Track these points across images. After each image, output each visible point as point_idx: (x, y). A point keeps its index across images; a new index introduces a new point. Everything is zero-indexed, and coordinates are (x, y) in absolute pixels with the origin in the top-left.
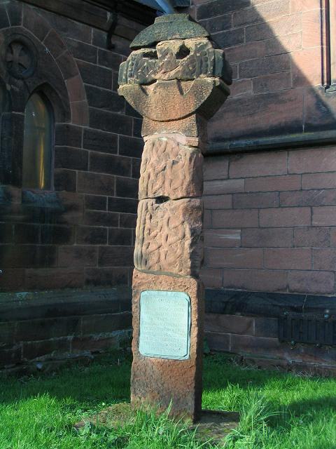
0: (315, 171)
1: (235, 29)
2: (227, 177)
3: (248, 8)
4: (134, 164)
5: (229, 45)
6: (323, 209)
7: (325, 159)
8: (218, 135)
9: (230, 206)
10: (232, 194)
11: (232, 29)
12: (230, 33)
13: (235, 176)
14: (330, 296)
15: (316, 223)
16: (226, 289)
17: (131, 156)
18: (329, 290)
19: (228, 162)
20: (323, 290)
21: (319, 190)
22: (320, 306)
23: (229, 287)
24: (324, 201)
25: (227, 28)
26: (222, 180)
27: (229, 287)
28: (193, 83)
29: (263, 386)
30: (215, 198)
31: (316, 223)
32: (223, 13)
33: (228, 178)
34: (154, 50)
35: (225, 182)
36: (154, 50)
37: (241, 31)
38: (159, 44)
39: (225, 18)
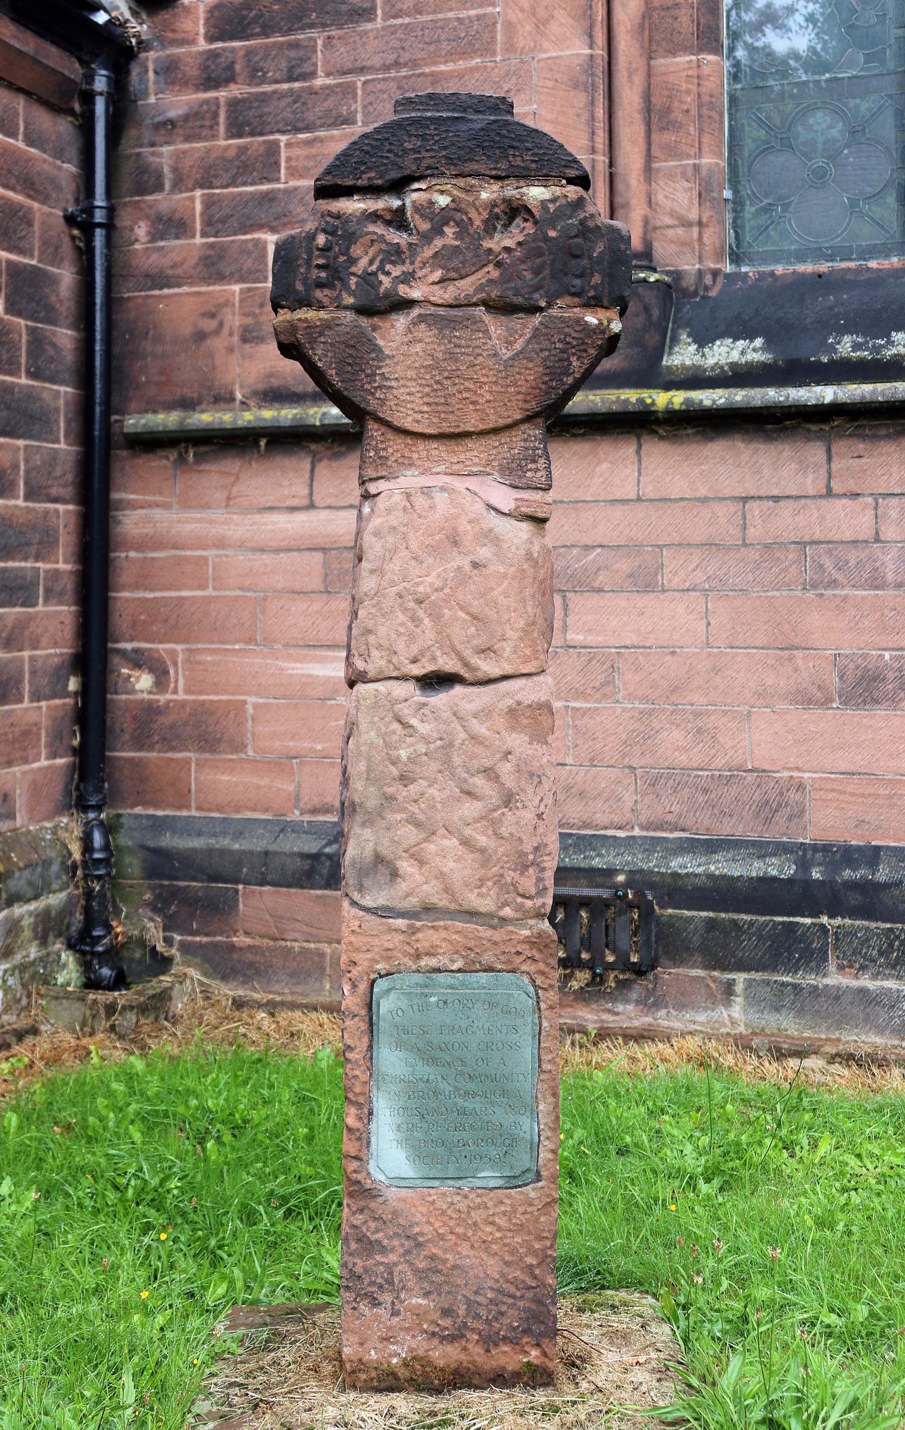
0: (575, 496)
1: (329, 81)
2: (305, 502)
3: (369, 26)
4: (27, 461)
5: (307, 128)
6: (595, 600)
7: (605, 466)
8: (275, 383)
9: (316, 583)
10: (323, 550)
11: (320, 81)
12: (312, 92)
13: (330, 501)
14: (621, 834)
15: (580, 637)
16: (307, 818)
17: (19, 437)
18: (616, 819)
19: (309, 460)
20: (601, 818)
21: (587, 548)
22: (597, 863)
23: (314, 811)
24: (601, 579)
25: (304, 77)
26: (293, 509)
27: (314, 811)
28: (537, 319)
29: (228, 982)
30: (268, 559)
31: (580, 637)
32: (288, 32)
33: (311, 506)
34: (396, 203)
35: (301, 517)
36: (396, 203)
37: (348, 91)
38: (416, 186)
39: (295, 45)
